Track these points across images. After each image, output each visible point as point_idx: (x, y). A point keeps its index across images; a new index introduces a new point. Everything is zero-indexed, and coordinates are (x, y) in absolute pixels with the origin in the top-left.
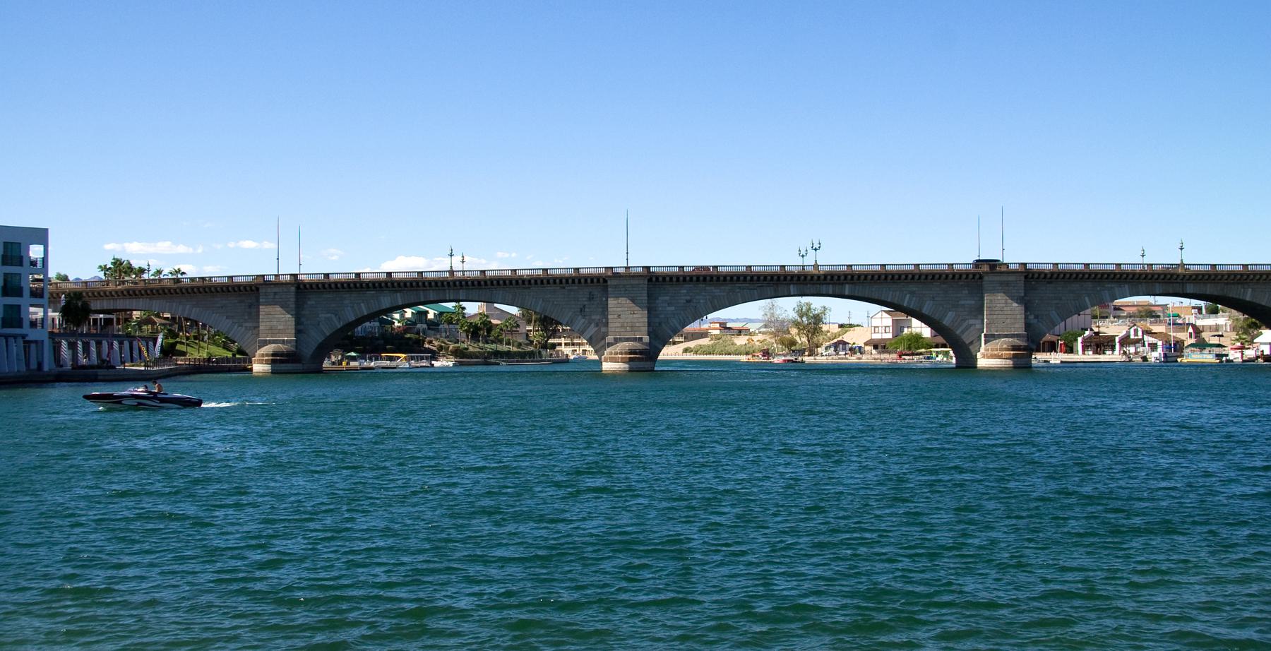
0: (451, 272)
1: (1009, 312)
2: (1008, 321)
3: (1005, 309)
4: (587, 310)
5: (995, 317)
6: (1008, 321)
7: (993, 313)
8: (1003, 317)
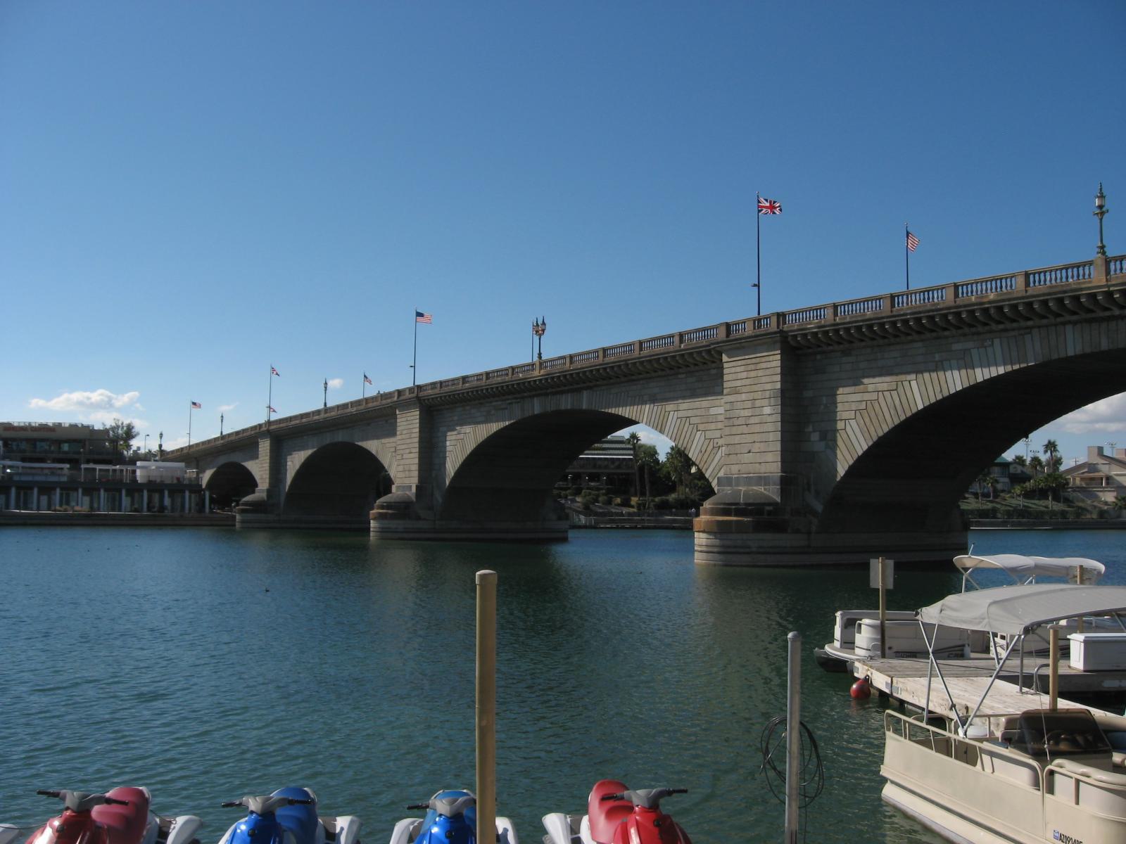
0: (542, 364)
1: (757, 428)
2: (756, 447)
3: (752, 420)
5: (737, 439)
6: (756, 447)
7: (734, 430)
8: (749, 438)
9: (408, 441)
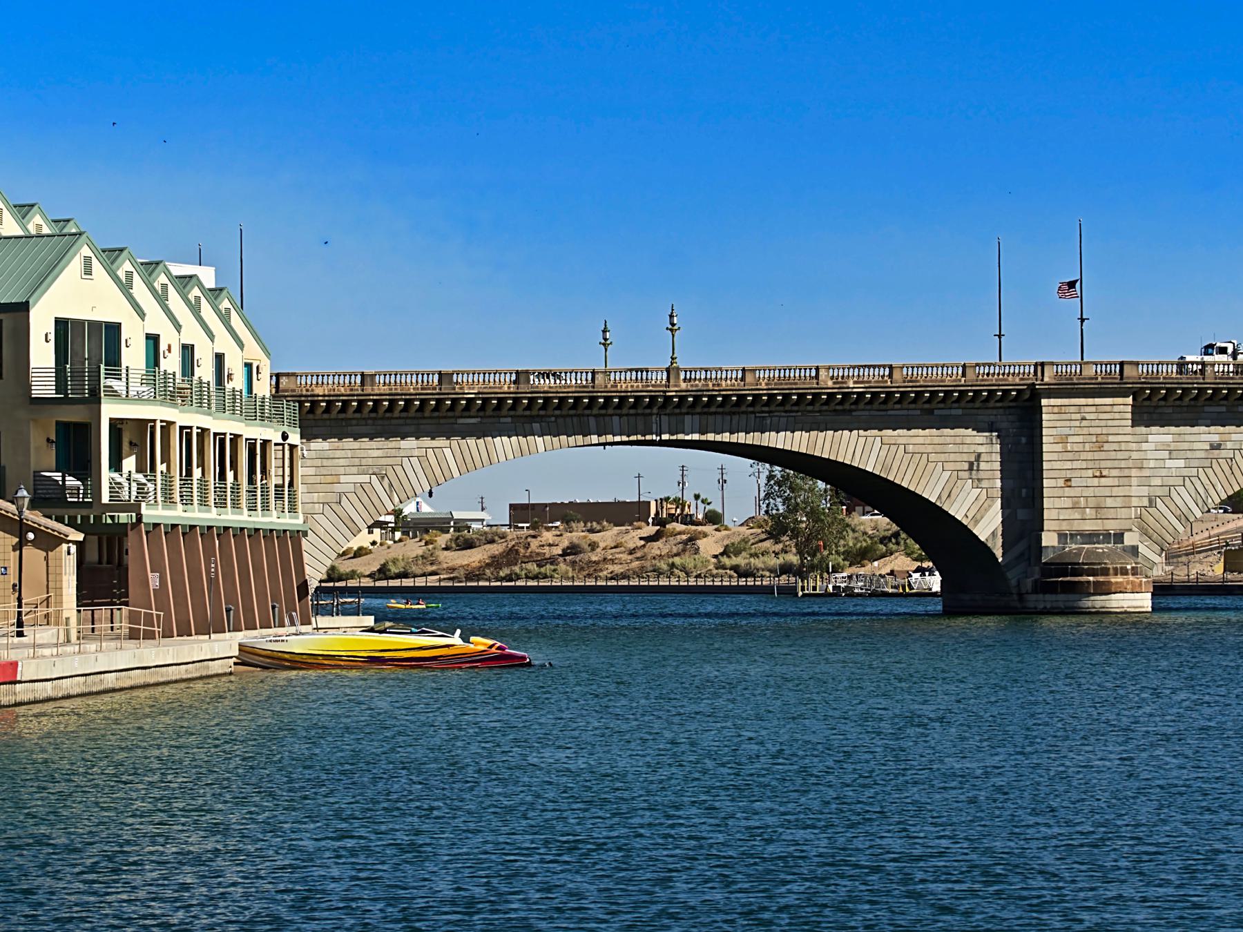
4: (983, 466)
9: (1090, 456)
